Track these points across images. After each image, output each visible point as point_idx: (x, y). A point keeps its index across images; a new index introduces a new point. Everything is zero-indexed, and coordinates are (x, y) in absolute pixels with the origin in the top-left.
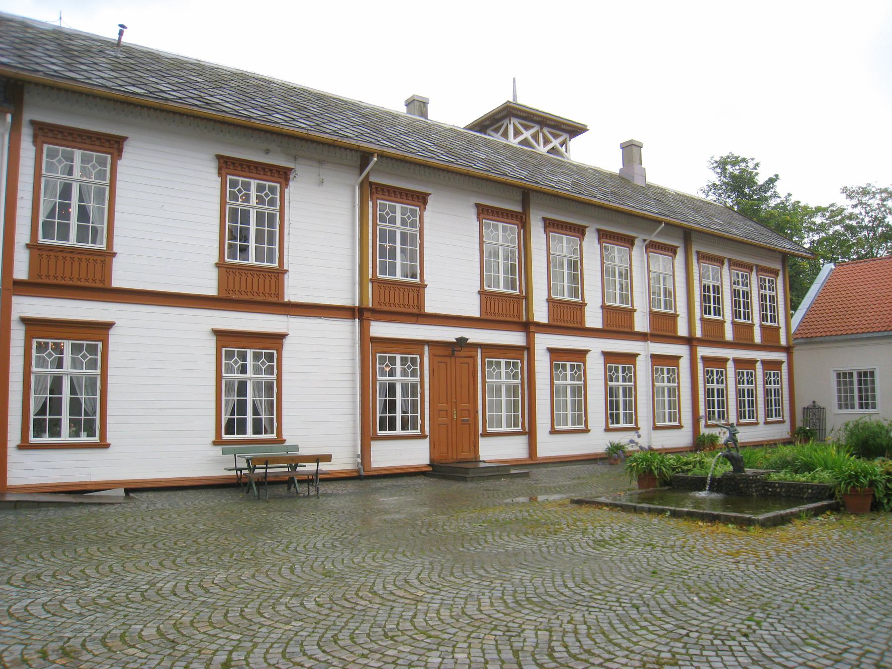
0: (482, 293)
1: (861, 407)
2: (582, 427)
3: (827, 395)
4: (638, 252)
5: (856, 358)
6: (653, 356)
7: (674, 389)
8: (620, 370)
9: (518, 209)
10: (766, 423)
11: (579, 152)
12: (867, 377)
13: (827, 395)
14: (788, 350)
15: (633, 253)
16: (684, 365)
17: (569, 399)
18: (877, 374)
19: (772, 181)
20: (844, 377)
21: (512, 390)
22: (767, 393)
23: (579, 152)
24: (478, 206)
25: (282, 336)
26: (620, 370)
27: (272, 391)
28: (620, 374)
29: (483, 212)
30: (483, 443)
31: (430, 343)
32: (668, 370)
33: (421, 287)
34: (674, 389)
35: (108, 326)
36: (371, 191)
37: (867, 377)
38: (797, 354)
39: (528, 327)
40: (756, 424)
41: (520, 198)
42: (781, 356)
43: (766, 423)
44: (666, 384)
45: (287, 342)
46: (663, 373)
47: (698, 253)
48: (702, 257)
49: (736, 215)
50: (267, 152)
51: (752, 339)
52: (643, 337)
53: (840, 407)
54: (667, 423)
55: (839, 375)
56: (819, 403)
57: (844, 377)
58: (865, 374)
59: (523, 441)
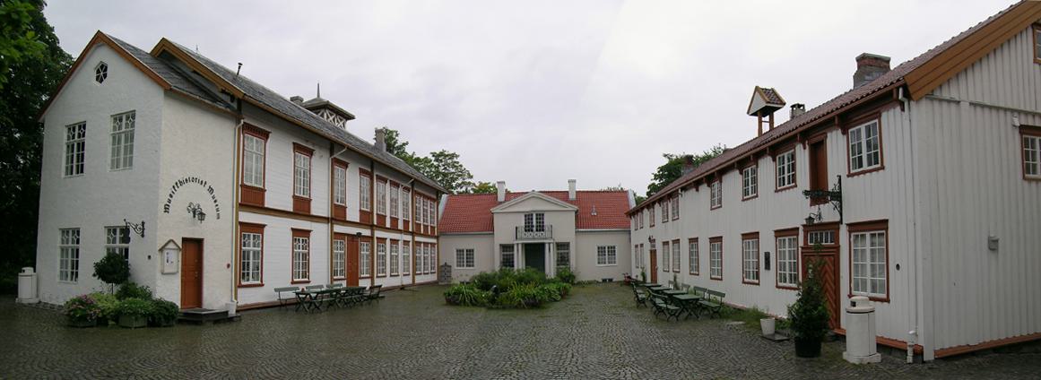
0: (294, 197)
1: (467, 266)
2: (259, 282)
3: (452, 259)
4: (400, 189)
5: (465, 243)
6: (294, 230)
7: (258, 253)
8: (252, 237)
9: (369, 170)
10: (391, 276)
11: (350, 127)
12: (470, 252)
13: (452, 259)
14: (437, 237)
15: (267, 144)
16: (411, 243)
17: (251, 261)
18: (475, 251)
19: (404, 144)
20: (460, 252)
21: (367, 256)
22: (391, 256)
23: (350, 127)
24: (360, 169)
25: (309, 231)
26: (252, 237)
27: (259, 255)
28: (252, 240)
29: (297, 147)
30: (360, 281)
31: (348, 235)
32: (254, 236)
33: (345, 208)
34: (258, 253)
35: (263, 226)
36: (336, 162)
37: (470, 252)
38: (441, 239)
39: (372, 227)
40: (385, 276)
41: (329, 147)
42: (434, 241)
43: (391, 276)
44: (301, 250)
45: (265, 229)
46: (249, 239)
47: (377, 175)
48: (379, 178)
49: (476, 197)
50: (307, 141)
51: (373, 222)
52: (400, 231)
53: (599, 263)
54: (301, 279)
55: (457, 251)
56: (93, 271)
57: (460, 252)
58: (470, 251)
59: (369, 280)
